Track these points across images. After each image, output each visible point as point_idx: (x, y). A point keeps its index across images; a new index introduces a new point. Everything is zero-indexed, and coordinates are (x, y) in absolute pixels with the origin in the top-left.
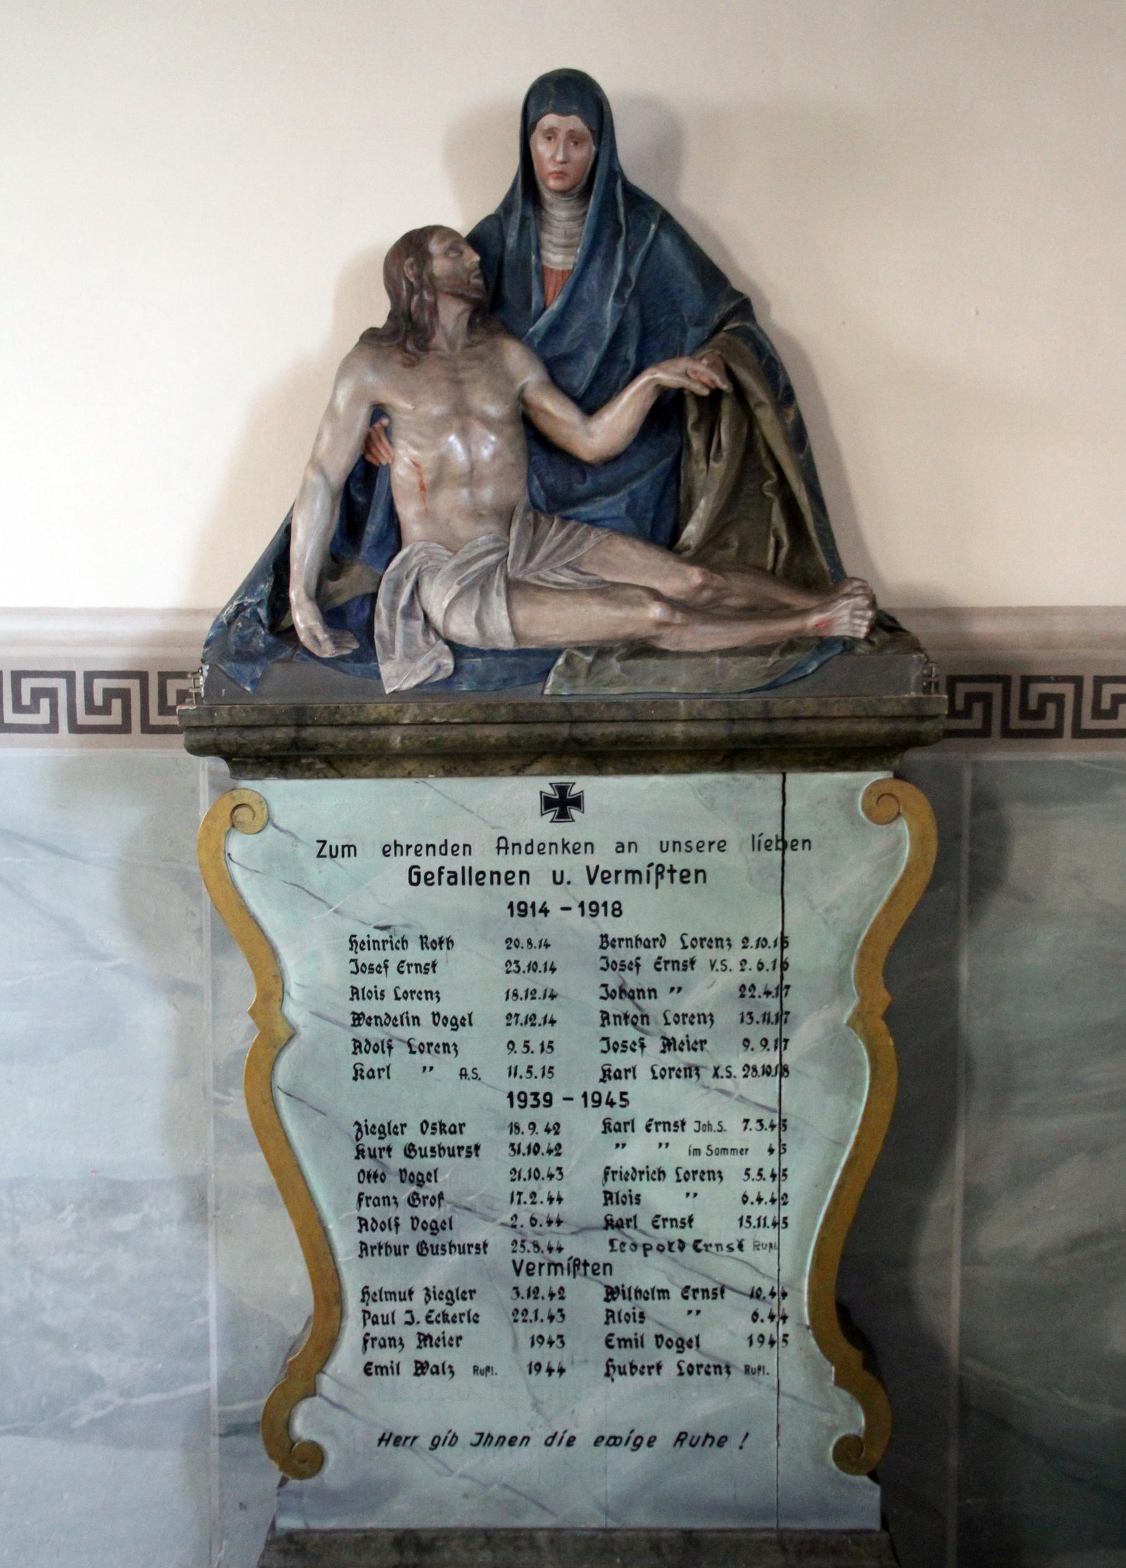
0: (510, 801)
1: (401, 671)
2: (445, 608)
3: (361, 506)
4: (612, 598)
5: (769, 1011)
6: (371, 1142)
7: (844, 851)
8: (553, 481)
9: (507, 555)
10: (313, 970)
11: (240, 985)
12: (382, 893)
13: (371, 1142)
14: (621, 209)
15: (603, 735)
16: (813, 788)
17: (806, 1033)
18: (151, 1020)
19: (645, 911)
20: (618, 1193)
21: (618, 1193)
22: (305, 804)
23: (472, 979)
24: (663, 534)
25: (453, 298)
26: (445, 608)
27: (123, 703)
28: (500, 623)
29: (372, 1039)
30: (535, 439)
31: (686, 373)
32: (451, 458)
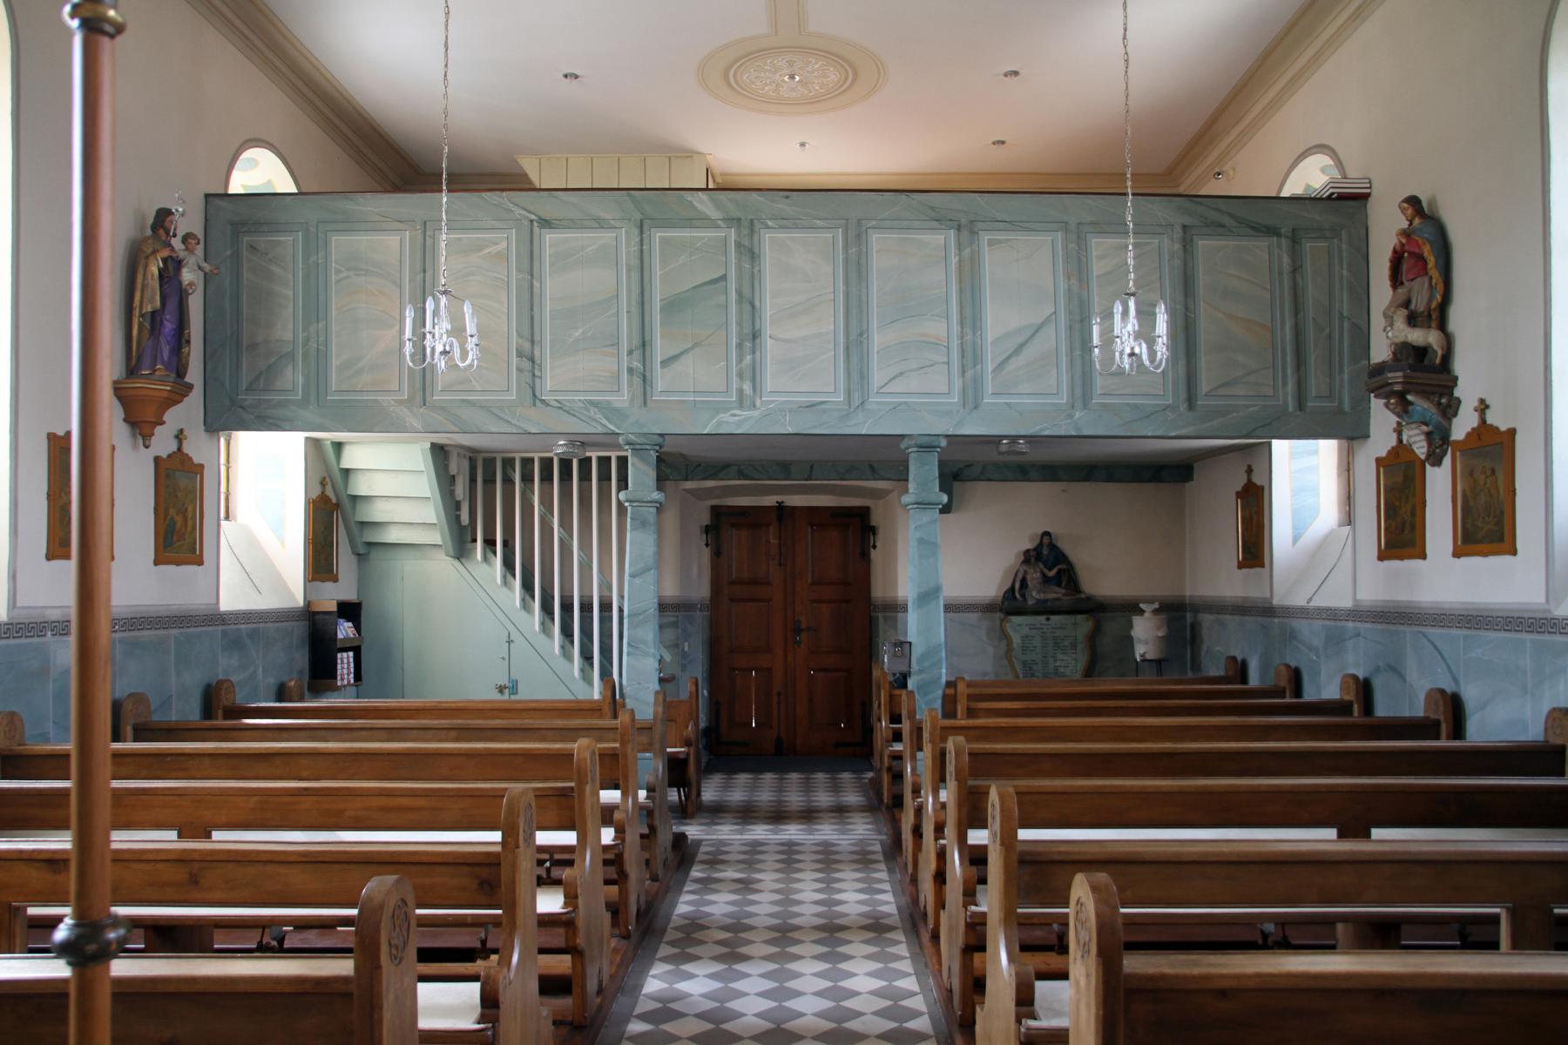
0: (1042, 618)
1: (1030, 602)
2: (1035, 595)
3: (1024, 582)
4: (1055, 593)
5: (1074, 646)
6: (1024, 663)
7: (1084, 625)
8: (1046, 580)
9: (591, 403)
10: (1016, 640)
11: (1004, 642)
12: (1026, 631)
13: (1024, 663)
14: (1053, 547)
15: (895, 608)
16: (1079, 617)
17: (1080, 647)
18: (991, 650)
19: (1058, 633)
20: (1056, 669)
21: (1056, 669)
22: (1016, 619)
23: (1037, 642)
24: (1059, 585)
25: (1029, 558)
26: (1035, 595)
27: (988, 608)
28: (1042, 596)
29: (1024, 649)
30: (1044, 575)
31: (1063, 566)
32: (1034, 576)
